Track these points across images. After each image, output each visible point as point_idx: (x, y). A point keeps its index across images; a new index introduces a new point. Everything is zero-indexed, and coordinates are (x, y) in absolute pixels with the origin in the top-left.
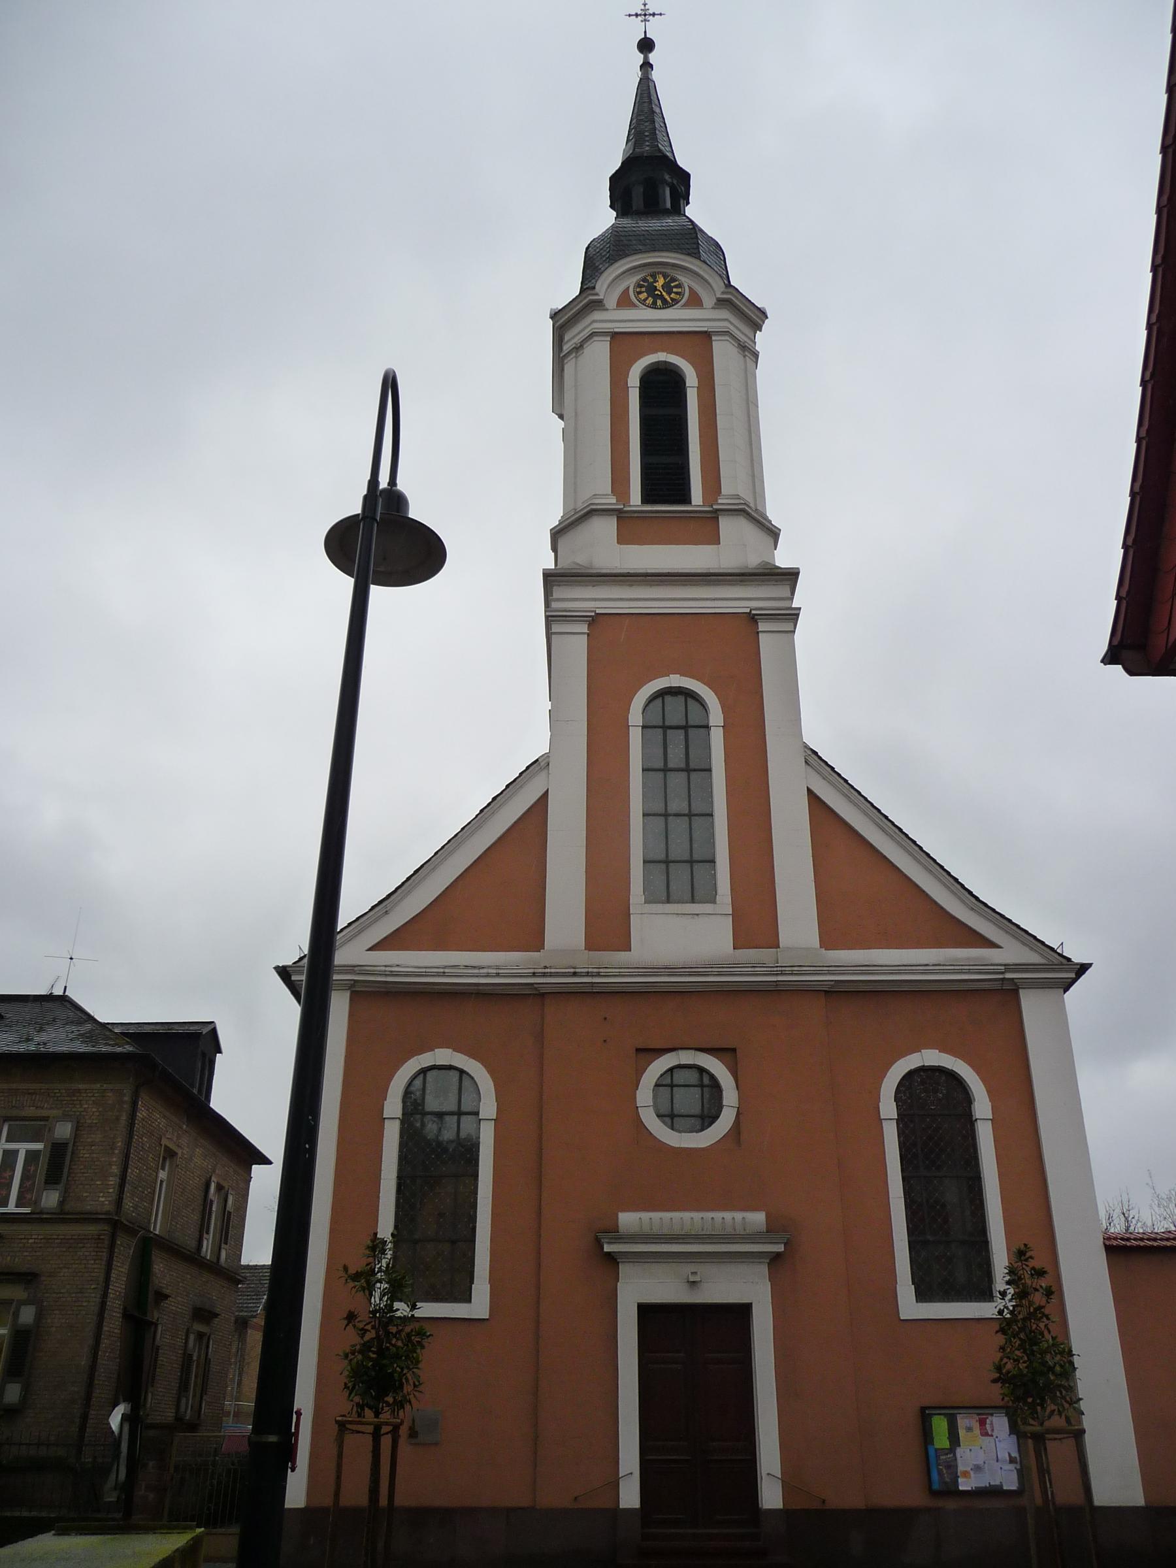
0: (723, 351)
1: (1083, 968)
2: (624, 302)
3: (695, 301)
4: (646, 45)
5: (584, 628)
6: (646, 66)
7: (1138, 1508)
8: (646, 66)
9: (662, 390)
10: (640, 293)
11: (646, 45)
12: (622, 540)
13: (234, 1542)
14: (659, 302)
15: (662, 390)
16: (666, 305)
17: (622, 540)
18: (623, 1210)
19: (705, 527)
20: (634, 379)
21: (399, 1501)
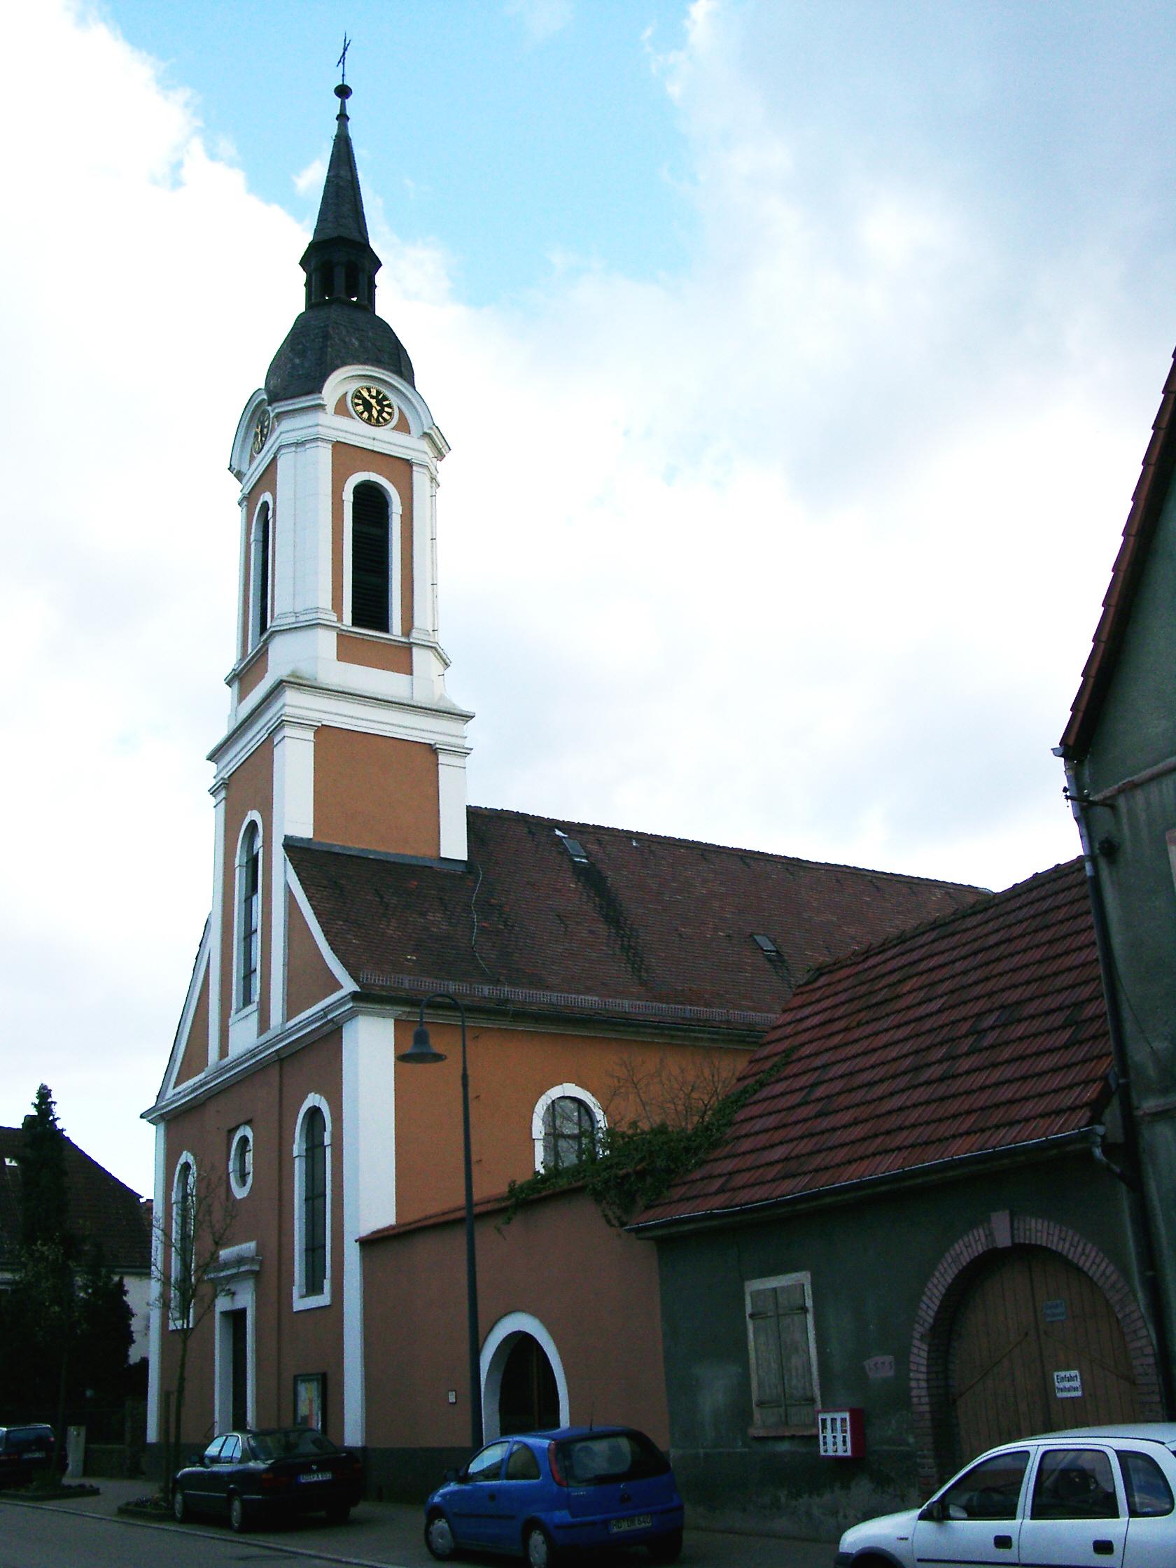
0: (420, 479)
1: (142, 1117)
2: (341, 409)
3: (403, 427)
4: (343, 92)
5: (310, 735)
6: (343, 117)
7: (1059, 872)
8: (343, 117)
9: (371, 506)
10: (357, 404)
11: (343, 92)
12: (341, 656)
13: (840, 1453)
14: (366, 415)
15: (371, 506)
16: (378, 424)
17: (341, 656)
18: (292, 1308)
19: (400, 658)
20: (348, 497)
21: (183, 1440)
